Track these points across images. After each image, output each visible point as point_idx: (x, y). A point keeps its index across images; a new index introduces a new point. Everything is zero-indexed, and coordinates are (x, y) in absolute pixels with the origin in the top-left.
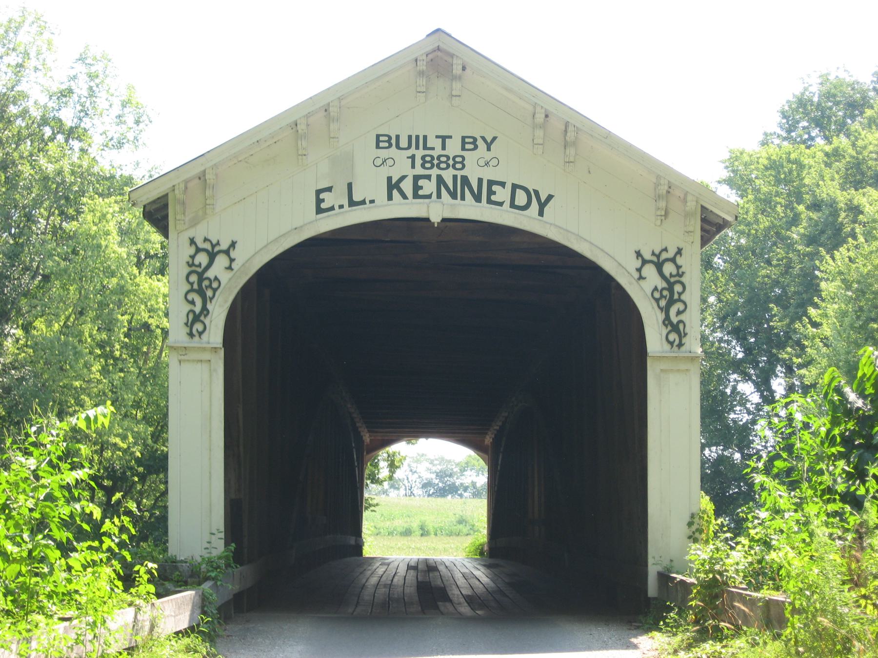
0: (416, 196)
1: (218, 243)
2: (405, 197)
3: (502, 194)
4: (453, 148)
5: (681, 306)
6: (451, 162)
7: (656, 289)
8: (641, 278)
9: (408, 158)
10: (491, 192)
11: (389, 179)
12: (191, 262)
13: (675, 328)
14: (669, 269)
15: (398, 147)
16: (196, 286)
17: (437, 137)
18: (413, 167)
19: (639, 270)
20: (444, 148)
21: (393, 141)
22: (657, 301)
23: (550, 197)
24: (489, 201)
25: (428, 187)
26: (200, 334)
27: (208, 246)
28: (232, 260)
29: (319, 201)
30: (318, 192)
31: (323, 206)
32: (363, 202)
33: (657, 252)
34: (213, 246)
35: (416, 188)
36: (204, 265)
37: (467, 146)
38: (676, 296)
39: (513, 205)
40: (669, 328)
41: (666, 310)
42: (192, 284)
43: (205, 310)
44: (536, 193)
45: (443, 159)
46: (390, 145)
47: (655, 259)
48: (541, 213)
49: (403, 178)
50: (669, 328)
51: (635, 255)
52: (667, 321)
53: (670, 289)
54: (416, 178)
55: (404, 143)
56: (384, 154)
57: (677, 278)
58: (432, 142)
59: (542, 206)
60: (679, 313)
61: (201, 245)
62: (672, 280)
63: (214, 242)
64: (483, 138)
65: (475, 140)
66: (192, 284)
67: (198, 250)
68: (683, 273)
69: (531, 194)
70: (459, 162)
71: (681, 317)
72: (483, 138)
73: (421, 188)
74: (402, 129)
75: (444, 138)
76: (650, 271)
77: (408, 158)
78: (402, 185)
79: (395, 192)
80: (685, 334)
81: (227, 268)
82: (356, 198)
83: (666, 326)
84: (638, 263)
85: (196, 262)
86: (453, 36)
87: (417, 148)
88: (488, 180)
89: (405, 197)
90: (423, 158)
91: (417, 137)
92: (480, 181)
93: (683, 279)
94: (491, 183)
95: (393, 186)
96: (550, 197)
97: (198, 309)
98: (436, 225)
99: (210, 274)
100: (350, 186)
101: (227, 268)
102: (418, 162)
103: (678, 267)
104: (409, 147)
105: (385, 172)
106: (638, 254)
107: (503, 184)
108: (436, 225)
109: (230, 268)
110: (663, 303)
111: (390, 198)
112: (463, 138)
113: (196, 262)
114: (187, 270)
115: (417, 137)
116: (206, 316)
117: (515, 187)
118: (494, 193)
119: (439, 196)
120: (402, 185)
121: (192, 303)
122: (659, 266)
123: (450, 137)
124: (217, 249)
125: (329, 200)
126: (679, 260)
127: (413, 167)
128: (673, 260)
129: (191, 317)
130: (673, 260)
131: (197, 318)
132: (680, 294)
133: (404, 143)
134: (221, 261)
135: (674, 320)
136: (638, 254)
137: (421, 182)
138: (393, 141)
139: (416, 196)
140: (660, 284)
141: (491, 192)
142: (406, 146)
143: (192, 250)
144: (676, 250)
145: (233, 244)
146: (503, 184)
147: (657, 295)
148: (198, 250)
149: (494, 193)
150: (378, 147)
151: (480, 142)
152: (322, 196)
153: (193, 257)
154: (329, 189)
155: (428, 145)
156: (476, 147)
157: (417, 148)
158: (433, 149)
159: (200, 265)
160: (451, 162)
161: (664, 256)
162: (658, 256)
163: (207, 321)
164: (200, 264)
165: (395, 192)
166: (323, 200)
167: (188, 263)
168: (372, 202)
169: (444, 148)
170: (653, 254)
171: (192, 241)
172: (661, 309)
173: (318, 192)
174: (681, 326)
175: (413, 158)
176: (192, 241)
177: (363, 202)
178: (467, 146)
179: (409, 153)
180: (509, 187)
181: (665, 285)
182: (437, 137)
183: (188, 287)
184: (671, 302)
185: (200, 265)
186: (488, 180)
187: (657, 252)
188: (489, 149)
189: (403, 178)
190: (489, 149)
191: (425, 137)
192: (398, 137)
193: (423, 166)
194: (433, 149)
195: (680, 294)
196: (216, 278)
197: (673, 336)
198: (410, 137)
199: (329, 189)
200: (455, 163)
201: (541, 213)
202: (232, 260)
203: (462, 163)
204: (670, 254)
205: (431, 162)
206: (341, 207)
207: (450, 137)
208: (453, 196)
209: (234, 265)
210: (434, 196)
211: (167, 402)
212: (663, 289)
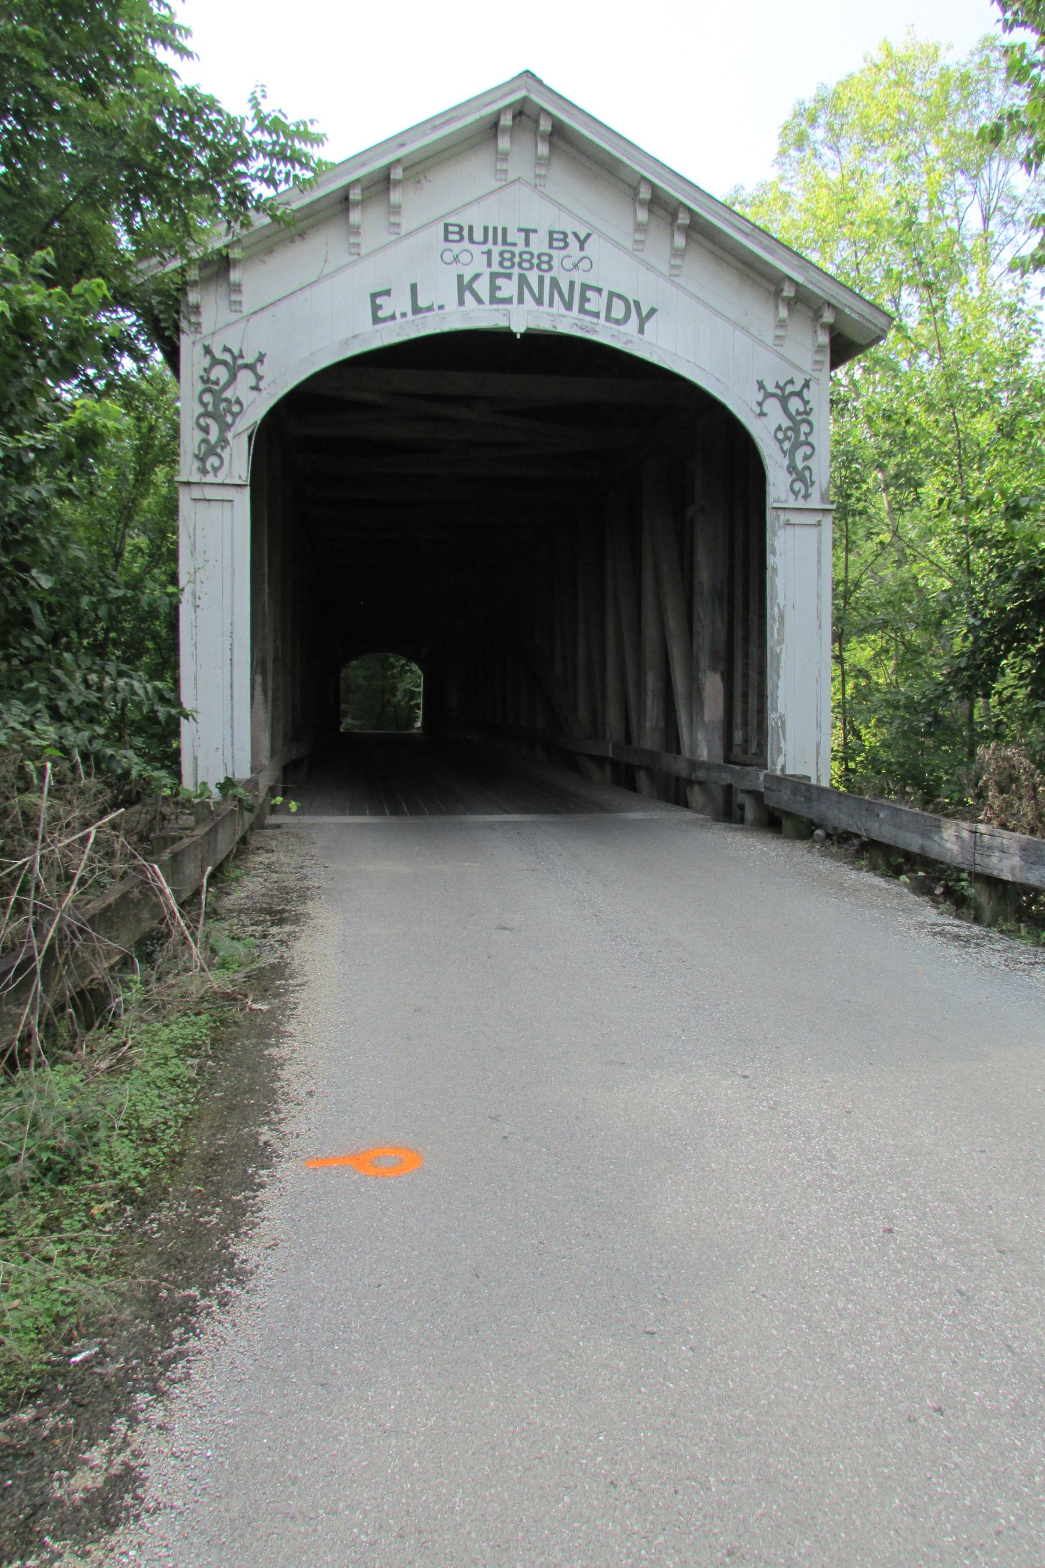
0: (494, 300)
1: (241, 356)
2: (480, 301)
3: (597, 303)
4: (539, 244)
5: (806, 450)
6: (535, 261)
7: (779, 428)
8: (762, 414)
9: (483, 253)
10: (584, 300)
11: (460, 278)
12: (205, 378)
13: (800, 476)
14: (795, 404)
15: (471, 240)
16: (210, 408)
17: (520, 230)
18: (489, 265)
19: (760, 404)
20: (527, 243)
21: (466, 233)
22: (780, 442)
23: (653, 311)
24: (582, 310)
25: (509, 288)
26: (216, 470)
27: (228, 357)
28: (259, 378)
29: (376, 308)
30: (374, 296)
31: (381, 314)
32: (430, 309)
33: (782, 384)
34: (235, 358)
35: (494, 288)
36: (222, 382)
37: (556, 244)
38: (802, 438)
39: (608, 318)
40: (794, 476)
41: (791, 454)
42: (205, 405)
43: (223, 441)
44: (637, 304)
45: (526, 257)
46: (462, 239)
47: (779, 392)
48: (641, 331)
49: (477, 276)
50: (794, 476)
51: (756, 386)
52: (792, 468)
53: (795, 429)
54: (494, 276)
55: (478, 236)
56: (456, 248)
57: (805, 416)
58: (514, 236)
59: (642, 321)
60: (806, 458)
61: (219, 355)
62: (799, 418)
63: (236, 353)
64: (575, 234)
65: (566, 235)
66: (205, 405)
67: (216, 362)
68: (811, 409)
69: (632, 306)
70: (545, 262)
71: (809, 463)
72: (575, 234)
73: (499, 288)
74: (476, 218)
75: (527, 232)
76: (772, 406)
77: (483, 253)
78: (475, 286)
79: (468, 295)
80: (813, 483)
81: (253, 388)
82: (422, 303)
83: (790, 473)
84: (760, 397)
85: (213, 377)
86: (545, 82)
87: (495, 242)
88: (582, 284)
89: (480, 301)
90: (501, 254)
91: (495, 229)
92: (572, 284)
93: (811, 418)
94: (585, 288)
95: (464, 287)
96: (653, 311)
97: (213, 438)
98: (518, 337)
99: (228, 394)
100: (414, 288)
101: (253, 388)
102: (496, 259)
103: (806, 403)
104: (485, 241)
105: (454, 270)
106: (761, 386)
107: (599, 291)
108: (518, 337)
109: (256, 388)
110: (787, 445)
111: (461, 302)
112: (551, 233)
113: (213, 377)
114: (201, 386)
115: (495, 229)
116: (223, 448)
117: (612, 295)
118: (588, 300)
119: (521, 301)
120: (475, 286)
121: (206, 430)
122: (784, 401)
123: (535, 231)
124: (240, 362)
125: (388, 306)
126: (806, 395)
127: (489, 265)
128: (799, 394)
129: (203, 448)
130: (799, 394)
131: (212, 451)
132: (807, 435)
133: (478, 236)
134: (246, 378)
135: (800, 465)
136: (761, 386)
137: (500, 282)
138: (466, 233)
139: (494, 300)
140: (786, 423)
141: (584, 300)
142: (481, 239)
143: (207, 362)
144: (803, 382)
145: (261, 359)
146: (599, 291)
147: (780, 436)
148: (216, 362)
149: (588, 300)
150: (446, 239)
151: (571, 239)
152: (379, 301)
153: (207, 371)
154: (387, 293)
155: (509, 240)
156: (566, 245)
157: (495, 242)
158: (514, 245)
159: (217, 383)
160: (535, 261)
161: (789, 389)
162: (782, 389)
163: (226, 454)
164: (218, 379)
165: (468, 295)
166: (380, 307)
167: (201, 377)
168: (441, 307)
169: (527, 243)
170: (777, 386)
171: (208, 351)
172: (784, 453)
173: (374, 296)
174: (807, 473)
175: (489, 253)
176: (208, 351)
177: (430, 309)
178: (556, 244)
179: (485, 248)
180: (605, 294)
181: (790, 424)
182: (520, 230)
183: (201, 410)
184: (796, 445)
185: (217, 383)
186: (582, 284)
187: (782, 384)
188: (582, 248)
189: (477, 276)
190: (582, 248)
191: (505, 230)
192: (471, 228)
193: (501, 264)
194: (514, 245)
195: (807, 435)
196: (238, 402)
197: (797, 486)
198: (486, 229)
199: (387, 293)
200: (541, 262)
201: (641, 331)
202: (259, 378)
203: (549, 263)
204: (797, 388)
205: (511, 260)
206: (404, 315)
207: (535, 231)
208: (539, 301)
209: (262, 385)
210: (515, 300)
211: (782, 448)
212: (789, 429)
